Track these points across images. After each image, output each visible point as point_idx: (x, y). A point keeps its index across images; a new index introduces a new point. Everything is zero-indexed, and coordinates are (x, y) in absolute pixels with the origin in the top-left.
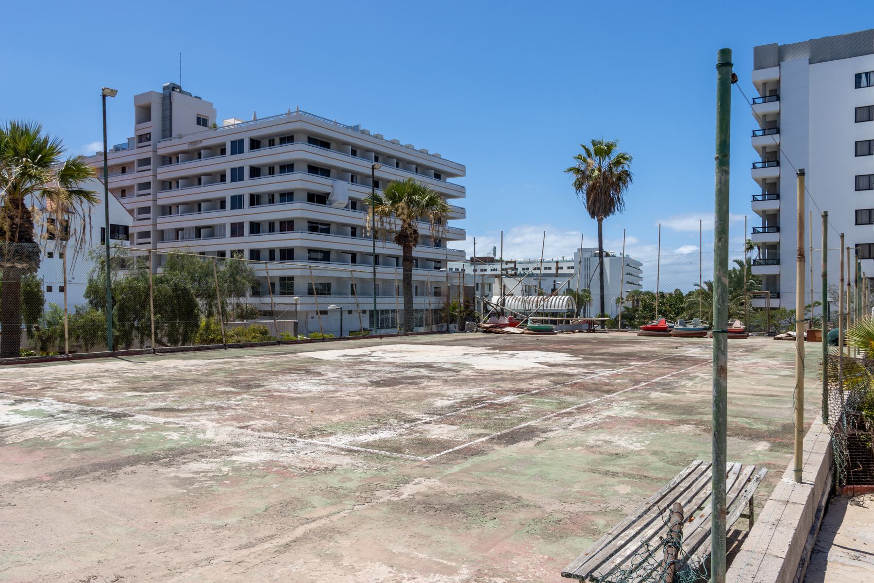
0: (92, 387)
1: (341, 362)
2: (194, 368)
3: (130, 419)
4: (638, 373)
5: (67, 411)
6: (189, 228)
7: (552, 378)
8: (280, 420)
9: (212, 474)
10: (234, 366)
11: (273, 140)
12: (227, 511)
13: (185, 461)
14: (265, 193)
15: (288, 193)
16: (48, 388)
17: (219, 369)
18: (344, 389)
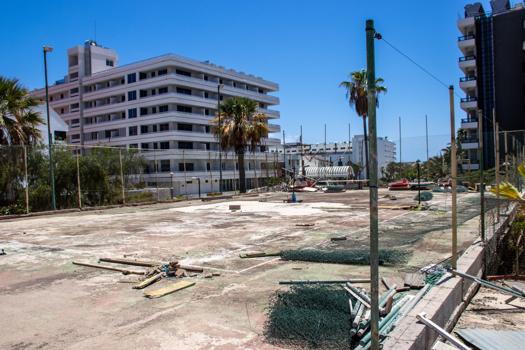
0: (41, 233)
1: (196, 214)
2: (104, 220)
3: (62, 252)
4: (383, 214)
5: (25, 248)
6: (102, 132)
7: (329, 219)
8: (153, 250)
9: (107, 283)
10: (128, 218)
11: (154, 73)
12: (114, 304)
13: (91, 276)
14: (150, 107)
16: (15, 234)
17: (119, 220)
18: (195, 230)
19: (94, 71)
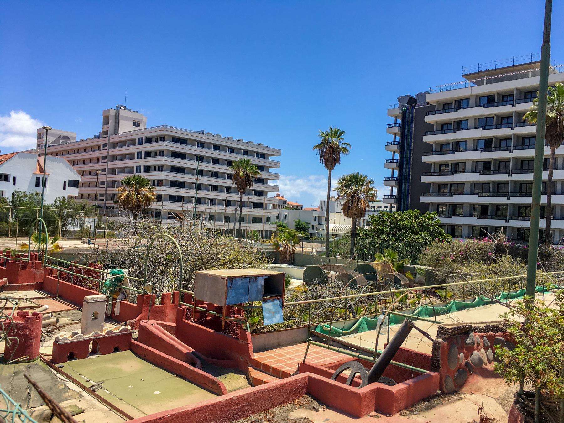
15: (261, 154)
19: (121, 131)
